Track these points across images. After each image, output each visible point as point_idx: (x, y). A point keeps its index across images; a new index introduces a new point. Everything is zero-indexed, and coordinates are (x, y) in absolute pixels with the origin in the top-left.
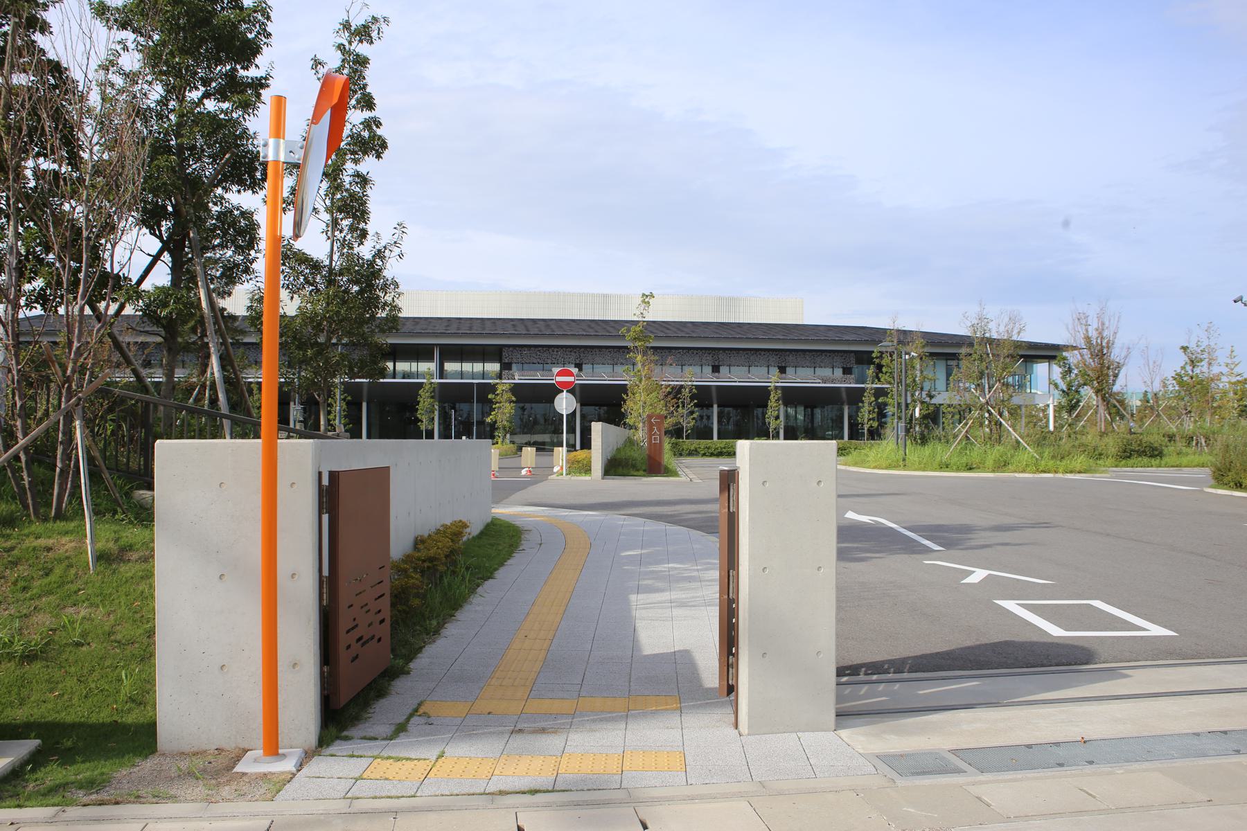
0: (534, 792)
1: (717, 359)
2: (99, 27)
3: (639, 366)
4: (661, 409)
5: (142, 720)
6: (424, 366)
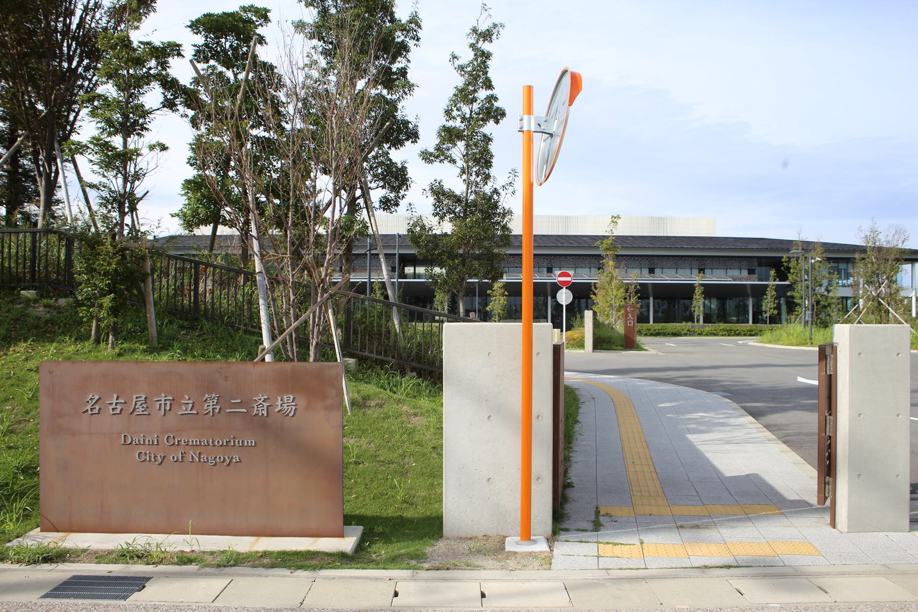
0: (729, 567)
1: (652, 263)
2: (300, 38)
5: (416, 515)
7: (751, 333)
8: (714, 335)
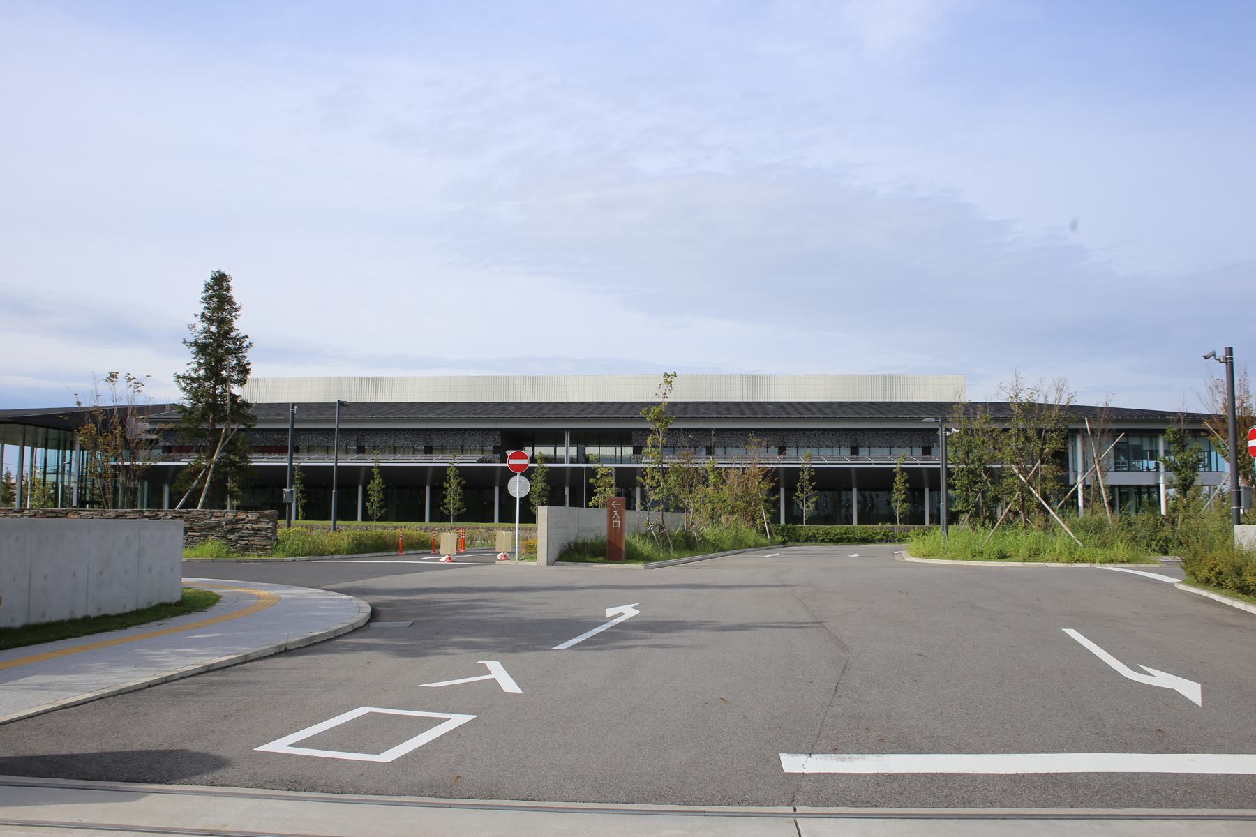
1: (855, 440)
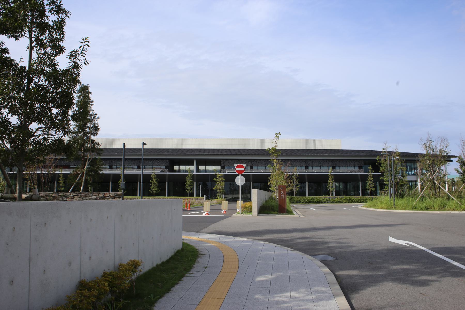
1: (307, 164)
3: (275, 165)
4: (284, 183)
6: (192, 168)
7: (361, 201)
8: (341, 202)
